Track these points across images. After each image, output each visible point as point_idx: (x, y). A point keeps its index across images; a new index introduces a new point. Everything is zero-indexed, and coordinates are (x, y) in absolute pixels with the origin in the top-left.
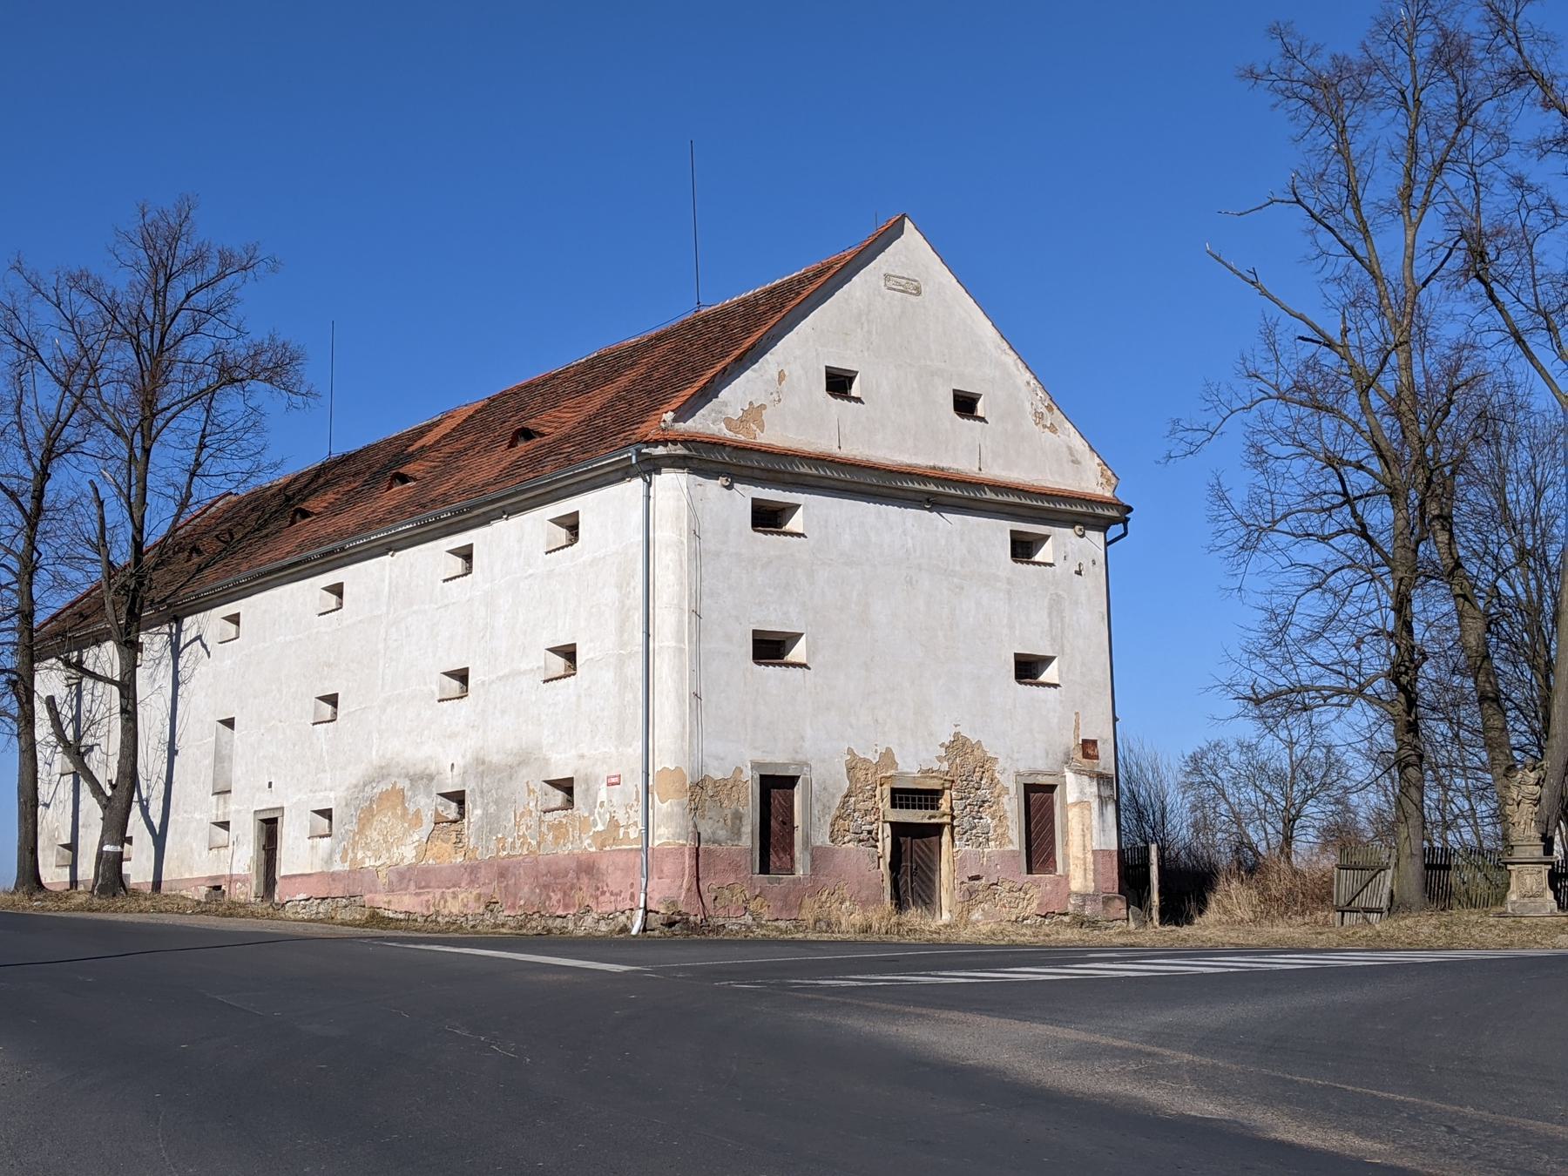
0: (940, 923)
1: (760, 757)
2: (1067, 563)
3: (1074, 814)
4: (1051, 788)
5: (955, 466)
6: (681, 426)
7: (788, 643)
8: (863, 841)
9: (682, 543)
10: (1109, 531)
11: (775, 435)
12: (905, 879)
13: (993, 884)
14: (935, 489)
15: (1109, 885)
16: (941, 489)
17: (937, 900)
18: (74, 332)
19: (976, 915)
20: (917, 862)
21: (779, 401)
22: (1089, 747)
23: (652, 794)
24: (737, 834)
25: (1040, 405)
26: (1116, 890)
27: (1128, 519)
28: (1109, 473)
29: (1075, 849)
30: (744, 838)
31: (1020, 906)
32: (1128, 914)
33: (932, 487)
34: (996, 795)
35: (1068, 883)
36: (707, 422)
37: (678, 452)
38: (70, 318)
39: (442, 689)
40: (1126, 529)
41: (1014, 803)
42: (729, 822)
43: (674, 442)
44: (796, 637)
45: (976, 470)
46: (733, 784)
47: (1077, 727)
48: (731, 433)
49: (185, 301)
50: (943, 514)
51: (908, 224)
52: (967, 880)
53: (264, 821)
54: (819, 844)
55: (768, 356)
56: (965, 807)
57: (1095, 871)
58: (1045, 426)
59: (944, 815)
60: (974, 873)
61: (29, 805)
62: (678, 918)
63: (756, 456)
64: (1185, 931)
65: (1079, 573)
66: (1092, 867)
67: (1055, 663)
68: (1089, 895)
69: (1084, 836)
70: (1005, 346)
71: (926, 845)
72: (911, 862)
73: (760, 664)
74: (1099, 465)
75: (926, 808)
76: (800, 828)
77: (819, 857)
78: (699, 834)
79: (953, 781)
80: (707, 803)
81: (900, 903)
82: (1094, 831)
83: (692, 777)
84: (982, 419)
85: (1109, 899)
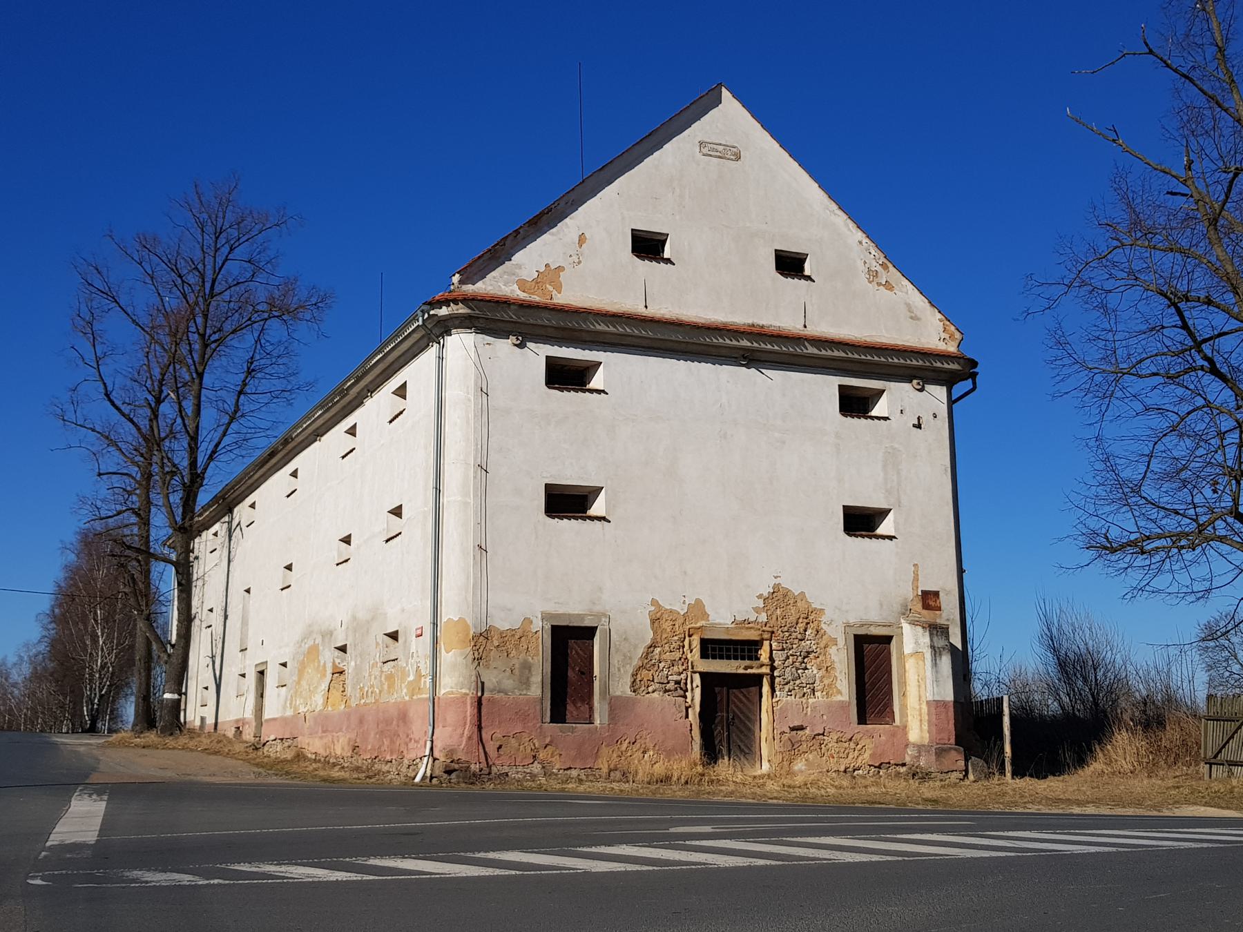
0: (759, 772)
1: (552, 608)
2: (904, 417)
3: (910, 665)
4: (887, 639)
5: (778, 324)
6: (469, 289)
7: (591, 497)
8: (670, 691)
9: (469, 400)
10: (955, 387)
11: (571, 295)
12: (719, 731)
13: (819, 735)
14: (749, 344)
15: (945, 736)
16: (755, 345)
17: (757, 750)
18: (154, 285)
19: (799, 765)
20: (734, 712)
21: (579, 262)
22: (929, 599)
23: (440, 645)
24: (526, 683)
25: (875, 264)
26: (953, 741)
27: (976, 374)
28: (953, 328)
29: (912, 700)
31: (851, 756)
32: (966, 765)
33: (745, 343)
34: (822, 645)
35: (906, 734)
36: (497, 283)
37: (460, 311)
38: (150, 273)
39: (340, 554)
40: (974, 383)
41: (843, 654)
42: (517, 672)
43: (455, 301)
44: (597, 491)
45: (801, 327)
46: (518, 636)
47: (916, 579)
48: (525, 294)
49: (229, 253)
50: (763, 371)
51: (725, 93)
52: (788, 730)
53: (259, 672)
54: (618, 693)
55: (567, 220)
56: (788, 658)
57: (929, 721)
58: (879, 284)
59: (762, 665)
60: (797, 723)
61: (142, 662)
62: (456, 766)
63: (545, 314)
64: (1052, 785)
65: (919, 426)
66: (927, 718)
67: (891, 516)
68: (924, 746)
69: (919, 686)
70: (834, 206)
71: (745, 696)
72: (728, 712)
73: (553, 517)
74: (940, 320)
75: (743, 658)
76: (598, 678)
77: (617, 707)
78: (483, 683)
79: (773, 632)
80: (492, 653)
81: (711, 753)
82: (928, 681)
83: (475, 627)
84: (809, 278)
85: (943, 750)
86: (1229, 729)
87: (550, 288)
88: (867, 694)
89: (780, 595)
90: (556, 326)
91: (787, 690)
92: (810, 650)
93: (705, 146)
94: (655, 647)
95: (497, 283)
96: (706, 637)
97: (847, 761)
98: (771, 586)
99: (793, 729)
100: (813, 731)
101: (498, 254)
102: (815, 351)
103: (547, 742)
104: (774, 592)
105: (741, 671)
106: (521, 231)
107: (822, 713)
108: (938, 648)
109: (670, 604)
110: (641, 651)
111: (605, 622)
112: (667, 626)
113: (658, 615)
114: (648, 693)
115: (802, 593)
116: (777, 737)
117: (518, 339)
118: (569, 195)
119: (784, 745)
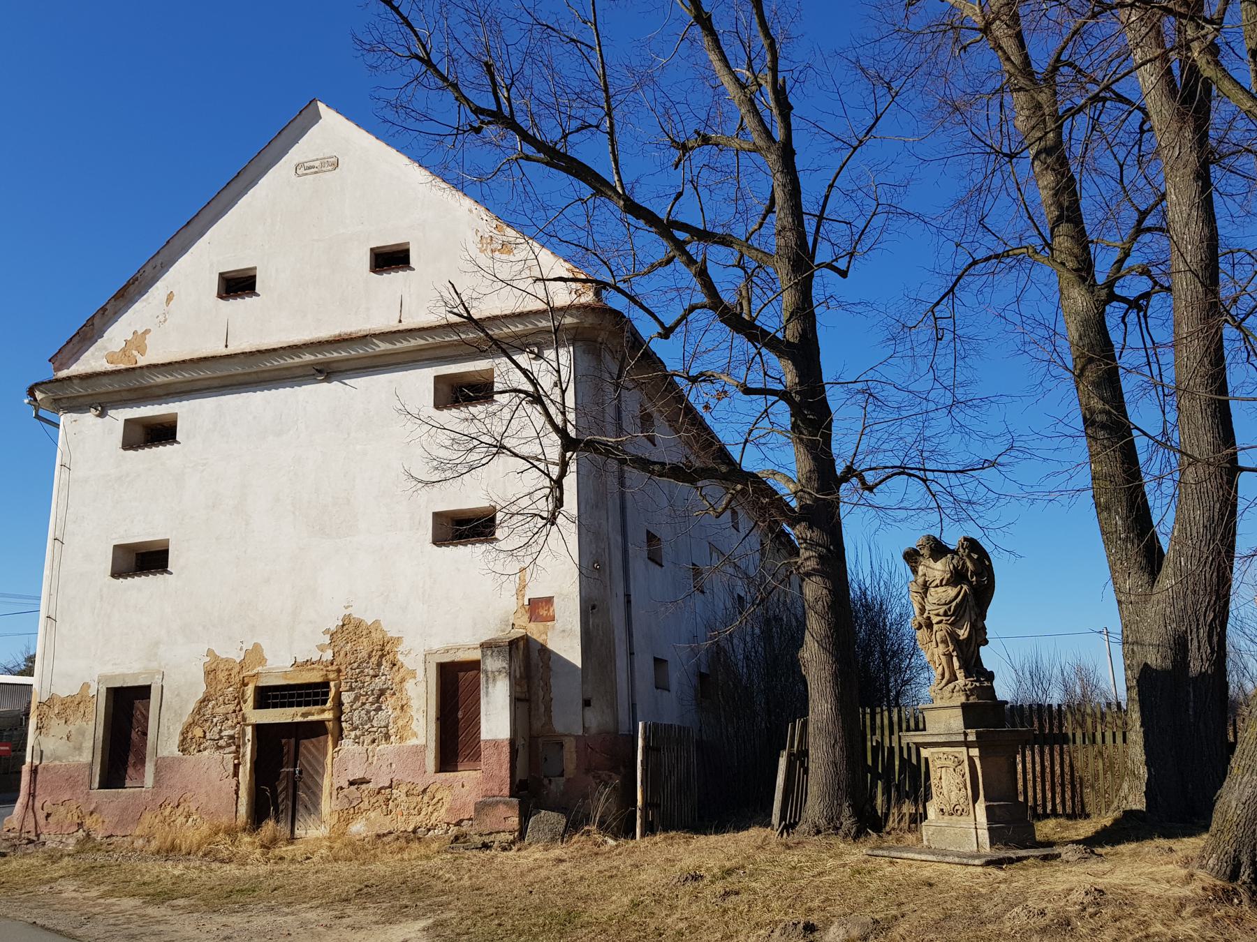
1: (109, 670)
11: (155, 354)
14: (313, 358)
16: (320, 356)
21: (165, 321)
24: (79, 748)
26: (506, 791)
30: (85, 755)
31: (423, 813)
33: (308, 358)
34: (397, 679)
36: (93, 361)
48: (112, 365)
51: (322, 107)
55: (158, 284)
60: (358, 775)
63: (105, 380)
71: (314, 746)
87: (135, 353)
88: (460, 734)
89: (351, 627)
90: (127, 388)
91: (353, 737)
92: (385, 686)
93: (303, 168)
94: (209, 701)
95: (93, 361)
96: (261, 685)
97: (419, 818)
98: (341, 618)
99: (352, 783)
100: (377, 784)
101: (87, 335)
102: (389, 346)
103: (92, 808)
104: (343, 625)
105: (299, 719)
106: (108, 307)
107: (389, 762)
108: (492, 672)
109: (227, 652)
110: (192, 706)
111: (158, 678)
112: (222, 676)
113: (213, 666)
114: (200, 751)
115: (377, 622)
116: (335, 793)
117: (97, 410)
118: (154, 259)
119: (341, 802)
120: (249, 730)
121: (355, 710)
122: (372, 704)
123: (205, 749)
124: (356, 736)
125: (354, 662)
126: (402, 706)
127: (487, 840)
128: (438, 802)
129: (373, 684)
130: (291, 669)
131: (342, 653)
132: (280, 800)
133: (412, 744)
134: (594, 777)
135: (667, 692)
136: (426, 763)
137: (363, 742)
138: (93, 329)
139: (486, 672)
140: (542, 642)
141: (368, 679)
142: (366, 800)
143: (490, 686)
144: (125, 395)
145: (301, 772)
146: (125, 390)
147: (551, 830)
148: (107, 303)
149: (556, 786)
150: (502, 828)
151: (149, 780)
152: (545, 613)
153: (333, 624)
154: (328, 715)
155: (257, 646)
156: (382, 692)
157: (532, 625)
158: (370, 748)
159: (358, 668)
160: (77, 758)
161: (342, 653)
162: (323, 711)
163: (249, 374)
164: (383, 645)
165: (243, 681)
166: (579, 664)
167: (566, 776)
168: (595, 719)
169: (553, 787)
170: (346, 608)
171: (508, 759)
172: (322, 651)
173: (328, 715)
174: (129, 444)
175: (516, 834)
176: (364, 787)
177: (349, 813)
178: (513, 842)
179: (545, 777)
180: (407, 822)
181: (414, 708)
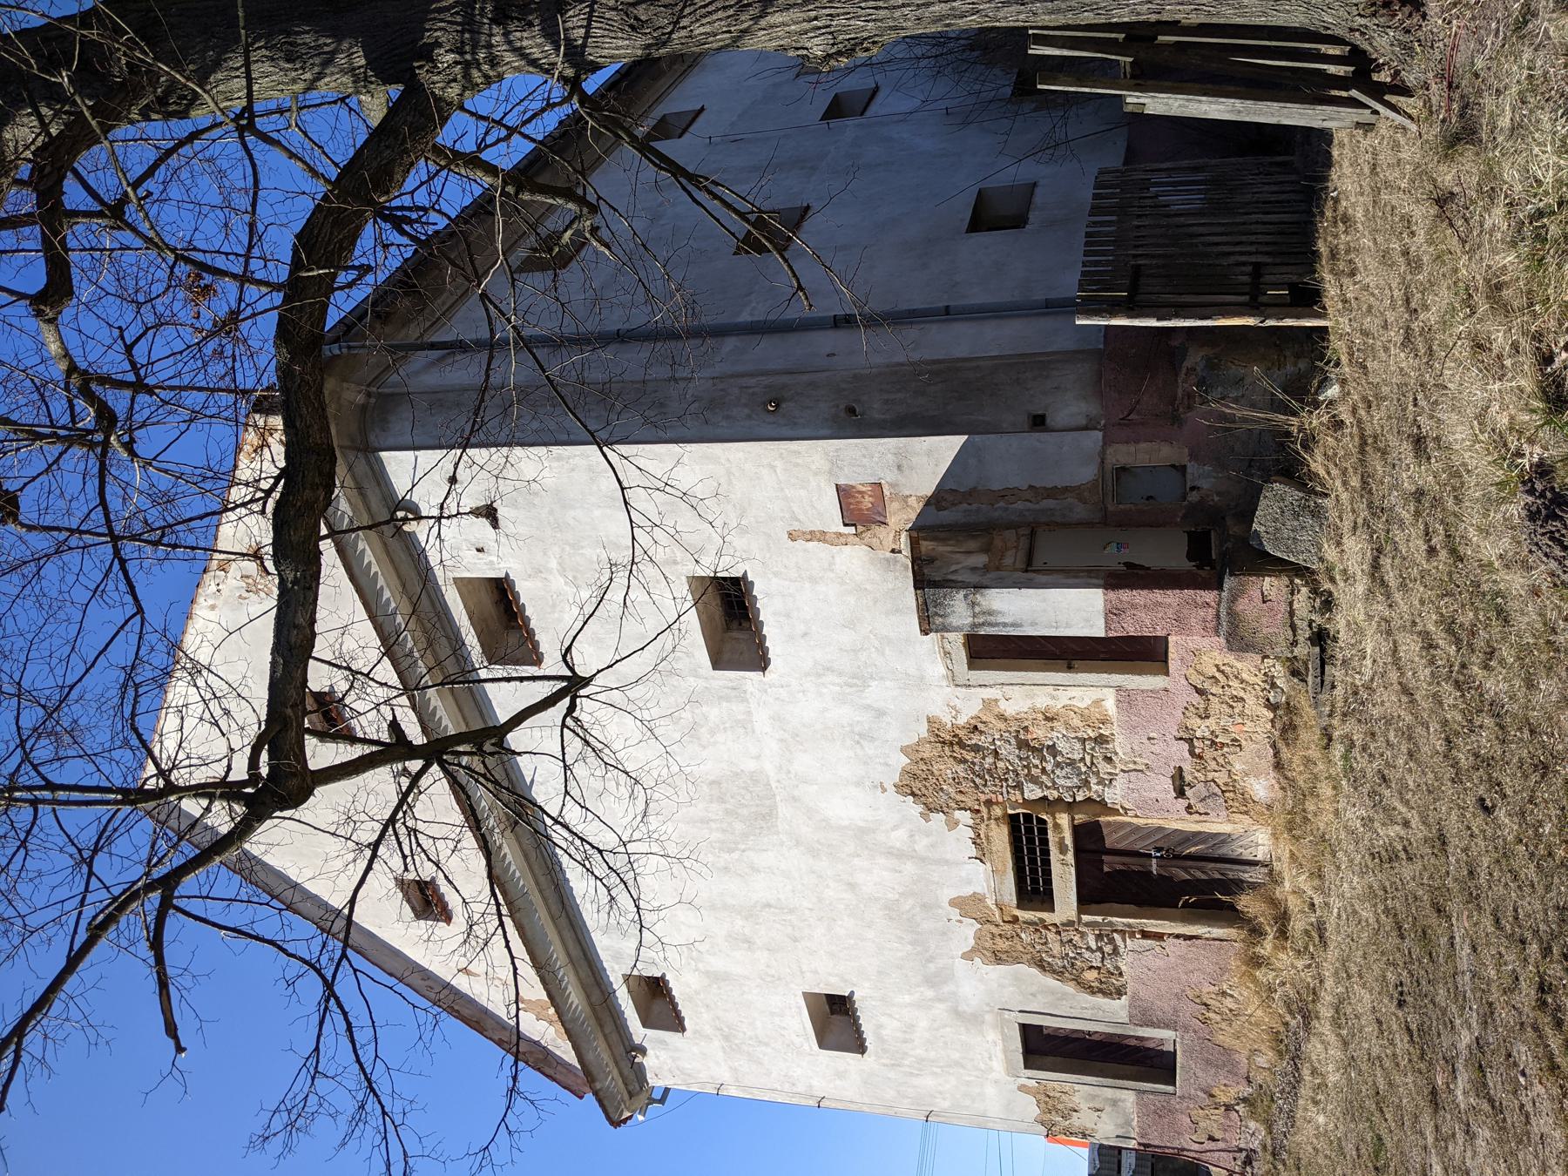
1: (998, 1065)
26: (1209, 596)
31: (1242, 694)
34: (1002, 726)
50: (528, 781)
60: (1168, 784)
86: (1232, 260)
92: (1013, 741)
94: (1042, 960)
97: (1250, 700)
98: (902, 798)
99: (1180, 793)
104: (913, 794)
105: (1070, 857)
107: (1146, 741)
108: (974, 616)
109: (966, 939)
110: (1050, 981)
112: (1002, 945)
113: (988, 954)
114: (1121, 974)
117: (635, 1057)
120: (1086, 918)
121: (1054, 783)
122: (1043, 759)
123: (1118, 968)
124: (1098, 784)
125: (974, 782)
126: (1047, 719)
127: (1304, 634)
128: (1223, 672)
129: (1010, 758)
130: (988, 864)
131: (959, 797)
132: (1204, 877)
133: (1114, 709)
134: (1190, 408)
135: (1038, 191)
136: (1150, 688)
137: (1110, 774)
138: (531, 1053)
139: (974, 625)
140: (921, 504)
141: (1001, 764)
142: (1210, 776)
143: (1001, 619)
144: (609, 1028)
145: (1158, 849)
146: (602, 1031)
147: (1296, 516)
148: (491, 1039)
149: (1206, 480)
150: (1284, 607)
151: (1167, 1034)
152: (867, 499)
153: (913, 809)
154: (1064, 819)
155: (954, 903)
156: (1023, 744)
157: (892, 520)
158: (1120, 766)
159: (982, 778)
160: (1129, 1105)
161: (959, 797)
162: (1057, 826)
163: (545, 899)
164: (944, 743)
165: (1009, 922)
166: (959, 440)
167: (1185, 460)
168: (1070, 407)
169: (1205, 484)
170: (884, 790)
171: (1144, 592)
172: (957, 823)
173: (1064, 819)
174: (676, 1023)
175: (1297, 581)
176: (1188, 778)
177: (1235, 798)
178: (1315, 591)
179: (1184, 498)
180: (1255, 719)
181: (1051, 702)
